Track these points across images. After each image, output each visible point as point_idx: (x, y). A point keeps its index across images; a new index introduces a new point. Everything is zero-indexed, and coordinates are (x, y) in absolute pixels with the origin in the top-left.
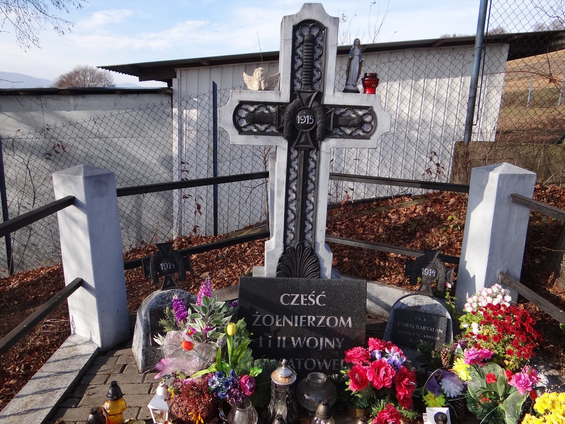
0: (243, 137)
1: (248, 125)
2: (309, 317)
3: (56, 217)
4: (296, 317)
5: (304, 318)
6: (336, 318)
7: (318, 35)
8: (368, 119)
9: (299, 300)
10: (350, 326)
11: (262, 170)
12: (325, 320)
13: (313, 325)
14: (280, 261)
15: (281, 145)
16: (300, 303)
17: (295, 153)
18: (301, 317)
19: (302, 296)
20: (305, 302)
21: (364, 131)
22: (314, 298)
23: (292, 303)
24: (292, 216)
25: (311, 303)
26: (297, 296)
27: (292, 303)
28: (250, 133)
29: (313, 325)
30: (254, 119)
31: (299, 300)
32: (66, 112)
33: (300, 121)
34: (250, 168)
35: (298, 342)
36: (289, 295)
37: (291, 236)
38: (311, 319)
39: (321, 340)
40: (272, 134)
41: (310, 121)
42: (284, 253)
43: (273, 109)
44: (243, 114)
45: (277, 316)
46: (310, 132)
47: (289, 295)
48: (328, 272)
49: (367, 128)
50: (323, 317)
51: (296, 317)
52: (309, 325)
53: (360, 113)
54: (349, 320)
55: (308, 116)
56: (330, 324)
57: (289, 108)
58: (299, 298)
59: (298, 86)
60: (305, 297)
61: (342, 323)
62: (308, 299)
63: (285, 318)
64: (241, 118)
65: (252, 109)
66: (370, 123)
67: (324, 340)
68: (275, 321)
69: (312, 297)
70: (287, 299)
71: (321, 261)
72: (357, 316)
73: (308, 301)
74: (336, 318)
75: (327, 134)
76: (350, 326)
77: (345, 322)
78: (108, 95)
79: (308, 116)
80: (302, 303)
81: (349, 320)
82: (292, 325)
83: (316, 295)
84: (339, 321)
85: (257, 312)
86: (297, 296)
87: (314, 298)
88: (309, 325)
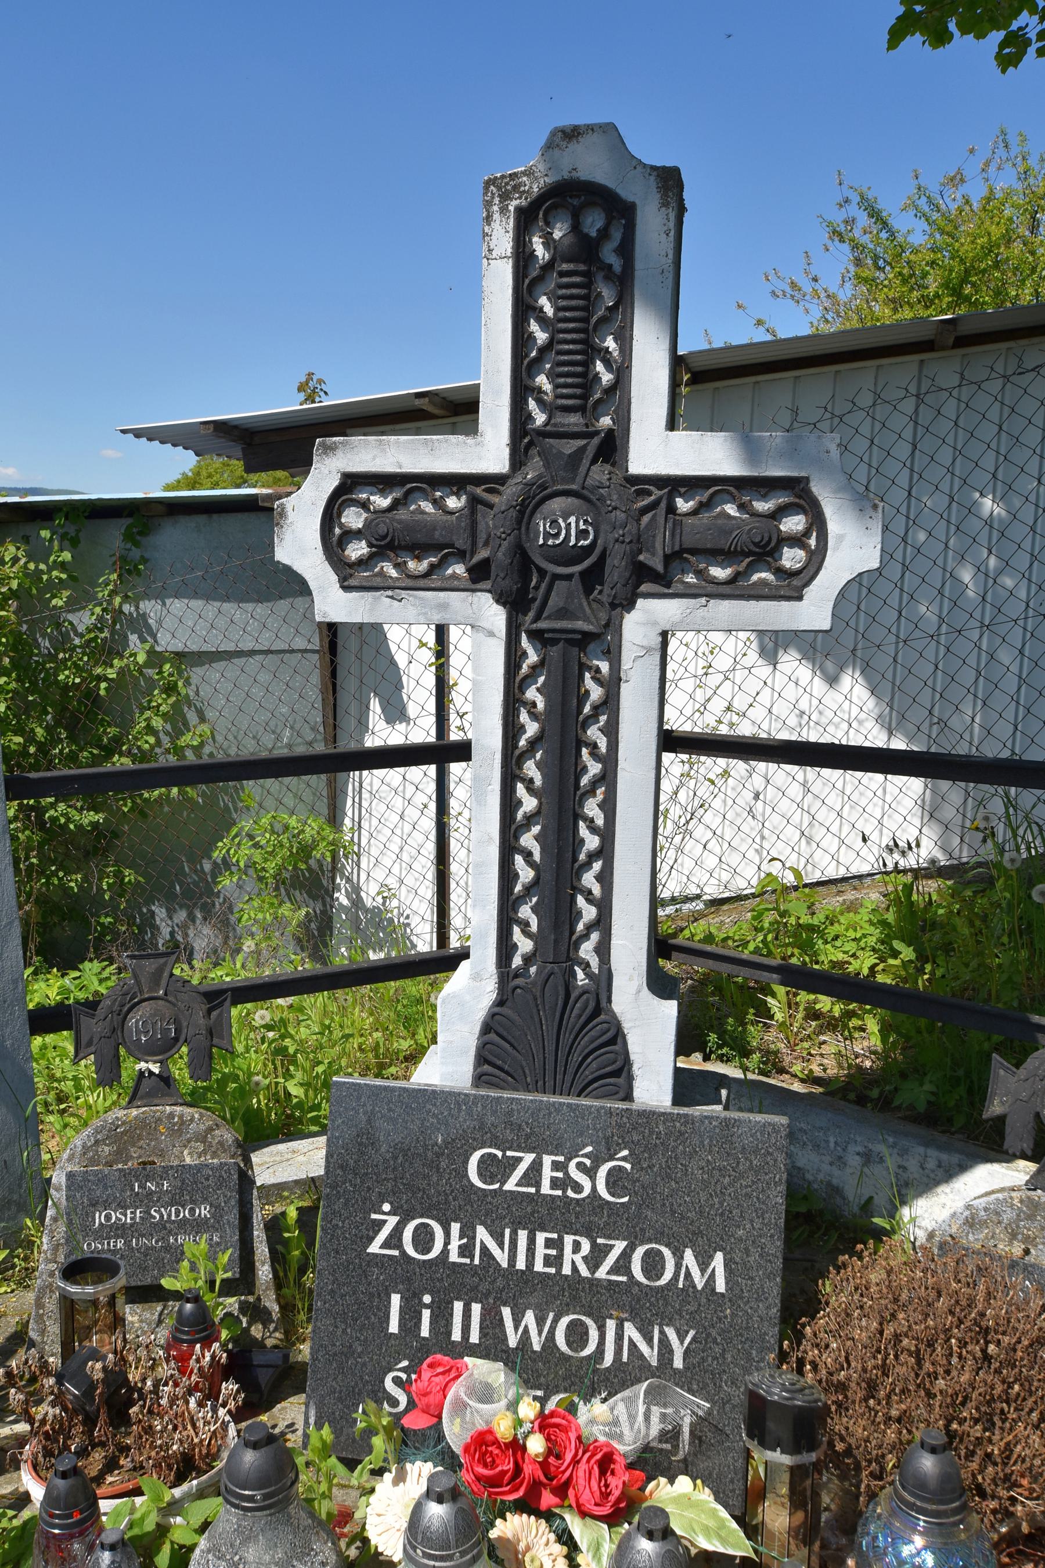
0: (811, 592)
1: (371, 556)
2: (569, 1240)
4: (523, 1235)
5: (549, 1243)
6: (667, 1252)
7: (604, 234)
9: (533, 1175)
10: (721, 1286)
13: (584, 1272)
14: (487, 1028)
16: (538, 1185)
18: (541, 1237)
19: (547, 1160)
20: (555, 1183)
22: (591, 1173)
23: (510, 1185)
25: (578, 1188)
26: (529, 1158)
27: (510, 1185)
29: (584, 1272)
31: (533, 1175)
32: (915, 749)
33: (547, 535)
35: (526, 1330)
36: (499, 1154)
37: (524, 945)
38: (577, 1247)
39: (611, 1325)
41: (582, 534)
42: (500, 1003)
45: (455, 1227)
46: (582, 574)
47: (499, 1154)
48: (653, 1086)
49: (792, 558)
50: (620, 1246)
51: (523, 1235)
52: (567, 1270)
53: (762, 506)
54: (718, 1261)
55: (572, 520)
56: (645, 1271)
57: (510, 492)
58: (536, 1167)
60: (556, 1167)
61: (688, 1274)
62: (566, 1174)
63: (482, 1233)
65: (382, 502)
66: (797, 541)
67: (620, 1329)
68: (447, 1243)
69: (580, 1166)
70: (492, 1169)
71: (1008, 1161)
72: (747, 1251)
73: (564, 1183)
74: (667, 1252)
76: (721, 1286)
77: (703, 1271)
78: (224, 515)
79: (572, 520)
80: (546, 1189)
81: (718, 1261)
82: (505, 1264)
83: (598, 1160)
84: (678, 1266)
85: (386, 1207)
86: (529, 1158)
87: (591, 1173)
88: (567, 1270)
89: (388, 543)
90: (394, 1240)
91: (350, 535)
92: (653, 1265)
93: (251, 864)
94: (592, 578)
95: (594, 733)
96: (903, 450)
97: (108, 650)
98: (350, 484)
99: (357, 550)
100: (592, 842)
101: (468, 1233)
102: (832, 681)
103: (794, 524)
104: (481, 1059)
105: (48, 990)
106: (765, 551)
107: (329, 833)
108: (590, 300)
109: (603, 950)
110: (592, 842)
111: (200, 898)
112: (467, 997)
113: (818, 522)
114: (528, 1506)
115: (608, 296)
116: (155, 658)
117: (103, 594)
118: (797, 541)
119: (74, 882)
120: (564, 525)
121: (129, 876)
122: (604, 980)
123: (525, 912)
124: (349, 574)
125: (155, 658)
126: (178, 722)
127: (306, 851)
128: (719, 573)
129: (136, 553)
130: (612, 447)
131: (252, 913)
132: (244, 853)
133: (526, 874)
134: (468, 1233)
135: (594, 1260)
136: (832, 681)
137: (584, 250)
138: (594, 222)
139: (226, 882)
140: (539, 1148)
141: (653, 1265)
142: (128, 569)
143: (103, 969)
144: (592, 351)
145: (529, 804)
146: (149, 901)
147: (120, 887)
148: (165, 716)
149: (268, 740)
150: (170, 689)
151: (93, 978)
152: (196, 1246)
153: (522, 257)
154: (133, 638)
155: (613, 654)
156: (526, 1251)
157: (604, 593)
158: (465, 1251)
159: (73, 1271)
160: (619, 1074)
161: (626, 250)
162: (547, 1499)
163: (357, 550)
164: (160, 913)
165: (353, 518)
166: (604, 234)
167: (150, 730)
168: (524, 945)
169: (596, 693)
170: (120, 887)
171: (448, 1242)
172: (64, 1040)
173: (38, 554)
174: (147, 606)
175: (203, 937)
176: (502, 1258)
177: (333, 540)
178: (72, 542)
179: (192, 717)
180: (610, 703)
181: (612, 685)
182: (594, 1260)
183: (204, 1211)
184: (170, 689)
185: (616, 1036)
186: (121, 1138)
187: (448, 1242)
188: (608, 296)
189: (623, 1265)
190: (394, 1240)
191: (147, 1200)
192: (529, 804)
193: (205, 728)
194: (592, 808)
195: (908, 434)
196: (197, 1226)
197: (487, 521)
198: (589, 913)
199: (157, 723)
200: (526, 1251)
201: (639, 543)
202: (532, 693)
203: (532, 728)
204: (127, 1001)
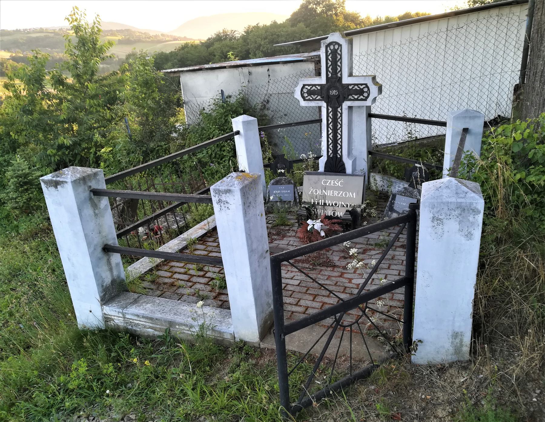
0: (368, 99)
3: (294, 353)
7: (338, 49)
8: (366, 90)
11: (317, 118)
12: (342, 194)
14: (326, 163)
15: (324, 104)
17: (330, 109)
21: (364, 96)
22: (338, 183)
24: (330, 141)
28: (309, 100)
30: (310, 93)
34: (426, 133)
40: (319, 100)
43: (319, 88)
44: (305, 90)
53: (362, 87)
57: (326, 86)
58: (331, 182)
59: (330, 75)
64: (304, 93)
65: (309, 88)
66: (366, 92)
75: (346, 99)
87: (338, 183)
92: (346, 194)
95: (339, 120)
98: (340, 45)
101: (322, 191)
104: (325, 168)
120: (334, 92)
122: (341, 156)
130: (340, 79)
134: (322, 191)
135: (338, 194)
141: (346, 194)
143: (329, 285)
144: (336, 65)
149: (311, 117)
158: (322, 193)
166: (338, 49)
182: (338, 194)
183: (289, 191)
185: (343, 165)
194: (339, 131)
195: (444, 43)
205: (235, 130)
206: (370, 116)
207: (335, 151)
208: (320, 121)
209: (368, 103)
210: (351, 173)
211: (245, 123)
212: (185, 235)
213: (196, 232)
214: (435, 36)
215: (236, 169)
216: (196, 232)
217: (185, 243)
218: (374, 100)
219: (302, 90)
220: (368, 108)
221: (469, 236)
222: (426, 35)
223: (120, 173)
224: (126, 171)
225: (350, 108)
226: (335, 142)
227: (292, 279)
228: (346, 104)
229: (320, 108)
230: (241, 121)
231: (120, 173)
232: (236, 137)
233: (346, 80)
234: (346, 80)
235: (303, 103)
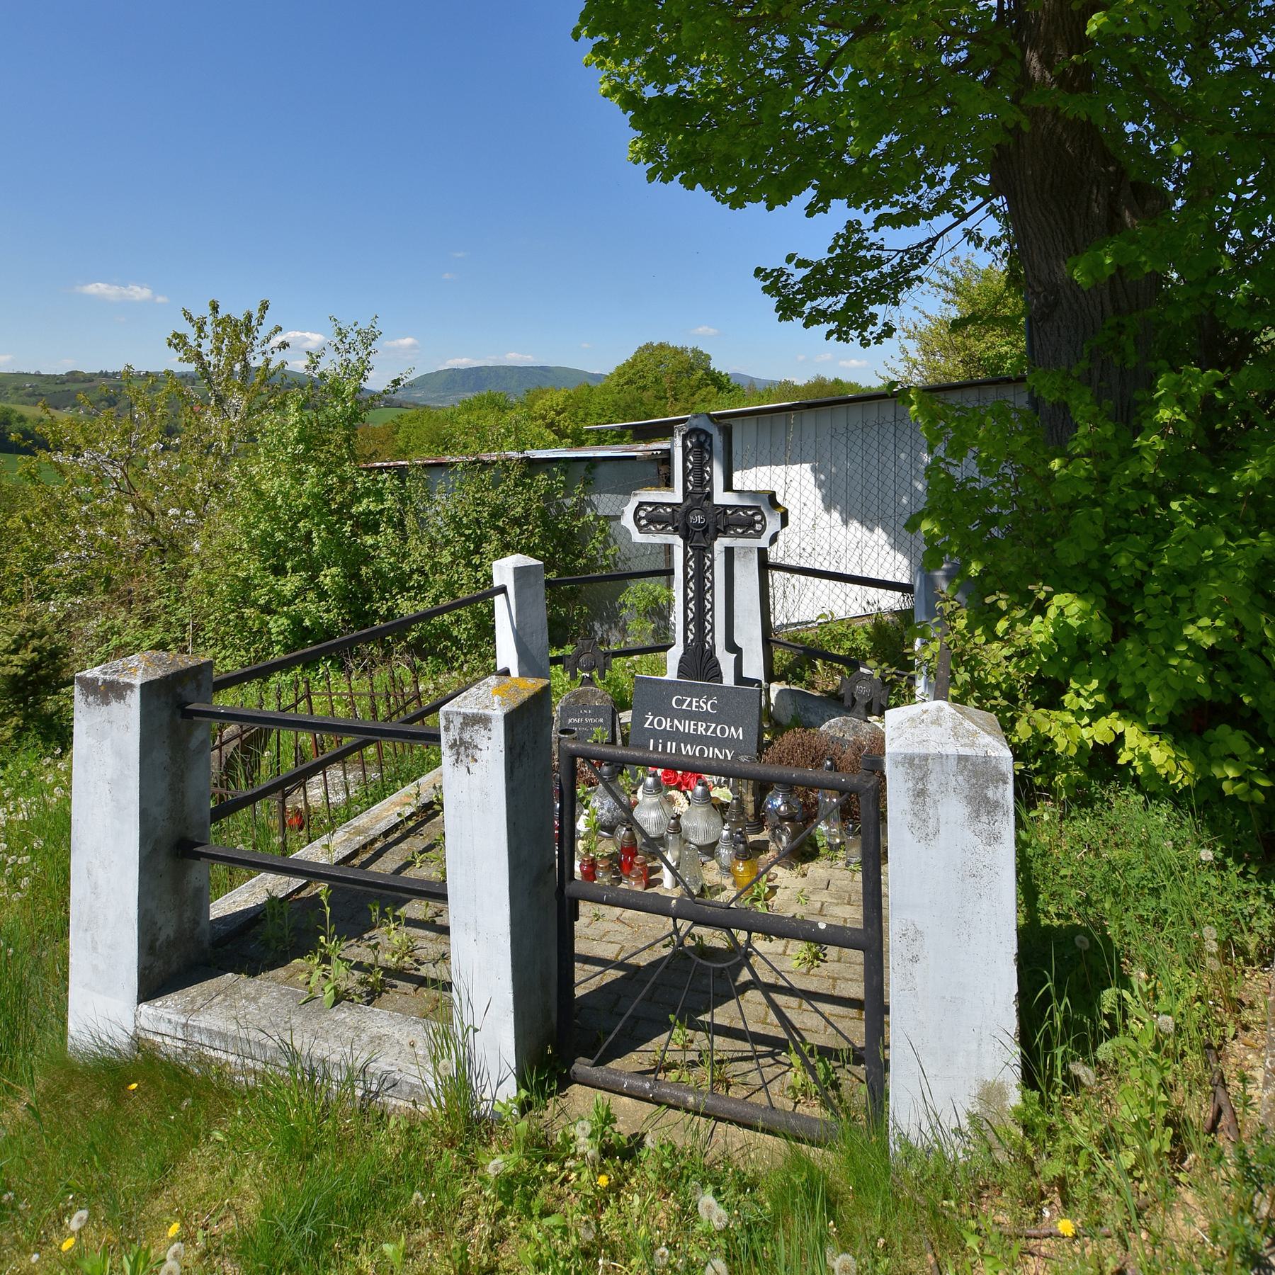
9: (690, 704)
15: (677, 542)
31: (690, 704)
34: (822, 587)
37: (691, 637)
49: (758, 527)
63: (676, 722)
65: (650, 509)
66: (759, 522)
70: (680, 702)
89: (652, 520)
90: (652, 723)
91: (641, 518)
93: (633, 605)
94: (705, 532)
96: (875, 444)
97: (578, 515)
98: (641, 504)
99: (643, 522)
100: (709, 606)
102: (872, 530)
103: (758, 518)
105: (554, 653)
106: (751, 524)
107: (666, 592)
108: (702, 458)
109: (713, 638)
110: (709, 606)
111: (613, 618)
112: (675, 655)
113: (764, 518)
114: (678, 788)
115: (707, 456)
116: (597, 518)
117: (577, 492)
118: (759, 522)
119: (563, 611)
120: (696, 518)
121: (585, 610)
123: (691, 626)
124: (641, 529)
125: (597, 518)
126: (606, 545)
127: (656, 599)
128: (739, 531)
129: (590, 476)
130: (709, 496)
131: (633, 626)
132: (630, 600)
133: (691, 615)
134: (672, 721)
135: (706, 730)
136: (872, 530)
137: (700, 445)
138: (702, 438)
139: (624, 612)
140: (692, 697)
142: (587, 483)
144: (703, 471)
145: (691, 595)
146: (593, 620)
147: (581, 614)
148: (600, 542)
150: (603, 531)
151: (569, 650)
152: (597, 730)
153: (684, 446)
154: (588, 510)
155: (712, 553)
156: (687, 727)
157: (708, 536)
158: (671, 727)
159: (563, 732)
160: (718, 676)
161: (711, 445)
162: (684, 788)
163: (643, 522)
164: (597, 625)
165: (642, 514)
167: (594, 548)
168: (691, 637)
169: (708, 563)
170: (581, 614)
171: (666, 724)
172: (560, 667)
173: (552, 477)
174: (594, 498)
175: (614, 636)
176: (681, 729)
177: (637, 520)
178: (565, 472)
179: (611, 540)
180: (712, 566)
181: (712, 561)
184: (603, 531)
185: (717, 664)
186: (577, 696)
187: (666, 724)
188: (707, 456)
189: (714, 731)
190: (652, 723)
191: (584, 716)
192: (691, 595)
193: (616, 547)
194: (708, 596)
196: (598, 725)
197: (677, 516)
198: (709, 627)
199: (597, 545)
200: (687, 727)
201: (717, 523)
202: (691, 563)
203: (691, 573)
204: (578, 655)
205: (496, 583)
206: (765, 566)
207: (701, 633)
208: (670, 572)
209: (764, 542)
210: (858, 956)
211: (520, 572)
212: (362, 821)
213: (388, 811)
214: (876, 428)
215: (491, 671)
216: (388, 811)
217: (360, 839)
218: (774, 539)
219: (636, 513)
220: (762, 553)
221: (995, 838)
222: (860, 426)
223: (315, 648)
224: (301, 652)
225: (729, 552)
226: (699, 618)
227: (600, 939)
228: (720, 544)
229: (669, 548)
230: (512, 566)
231: (315, 648)
232: (499, 600)
233: (721, 497)
234: (721, 497)
235: (637, 537)
